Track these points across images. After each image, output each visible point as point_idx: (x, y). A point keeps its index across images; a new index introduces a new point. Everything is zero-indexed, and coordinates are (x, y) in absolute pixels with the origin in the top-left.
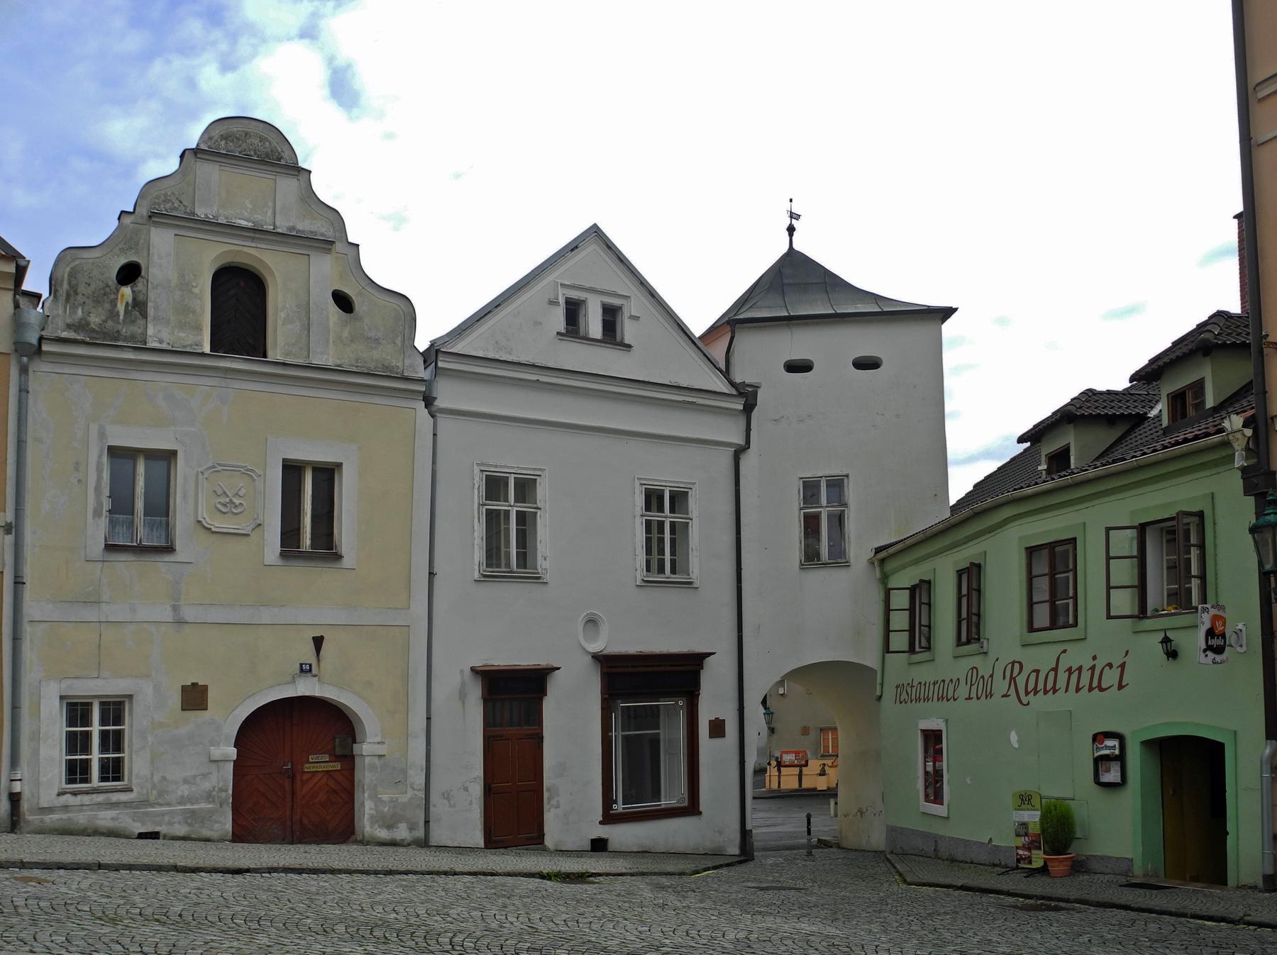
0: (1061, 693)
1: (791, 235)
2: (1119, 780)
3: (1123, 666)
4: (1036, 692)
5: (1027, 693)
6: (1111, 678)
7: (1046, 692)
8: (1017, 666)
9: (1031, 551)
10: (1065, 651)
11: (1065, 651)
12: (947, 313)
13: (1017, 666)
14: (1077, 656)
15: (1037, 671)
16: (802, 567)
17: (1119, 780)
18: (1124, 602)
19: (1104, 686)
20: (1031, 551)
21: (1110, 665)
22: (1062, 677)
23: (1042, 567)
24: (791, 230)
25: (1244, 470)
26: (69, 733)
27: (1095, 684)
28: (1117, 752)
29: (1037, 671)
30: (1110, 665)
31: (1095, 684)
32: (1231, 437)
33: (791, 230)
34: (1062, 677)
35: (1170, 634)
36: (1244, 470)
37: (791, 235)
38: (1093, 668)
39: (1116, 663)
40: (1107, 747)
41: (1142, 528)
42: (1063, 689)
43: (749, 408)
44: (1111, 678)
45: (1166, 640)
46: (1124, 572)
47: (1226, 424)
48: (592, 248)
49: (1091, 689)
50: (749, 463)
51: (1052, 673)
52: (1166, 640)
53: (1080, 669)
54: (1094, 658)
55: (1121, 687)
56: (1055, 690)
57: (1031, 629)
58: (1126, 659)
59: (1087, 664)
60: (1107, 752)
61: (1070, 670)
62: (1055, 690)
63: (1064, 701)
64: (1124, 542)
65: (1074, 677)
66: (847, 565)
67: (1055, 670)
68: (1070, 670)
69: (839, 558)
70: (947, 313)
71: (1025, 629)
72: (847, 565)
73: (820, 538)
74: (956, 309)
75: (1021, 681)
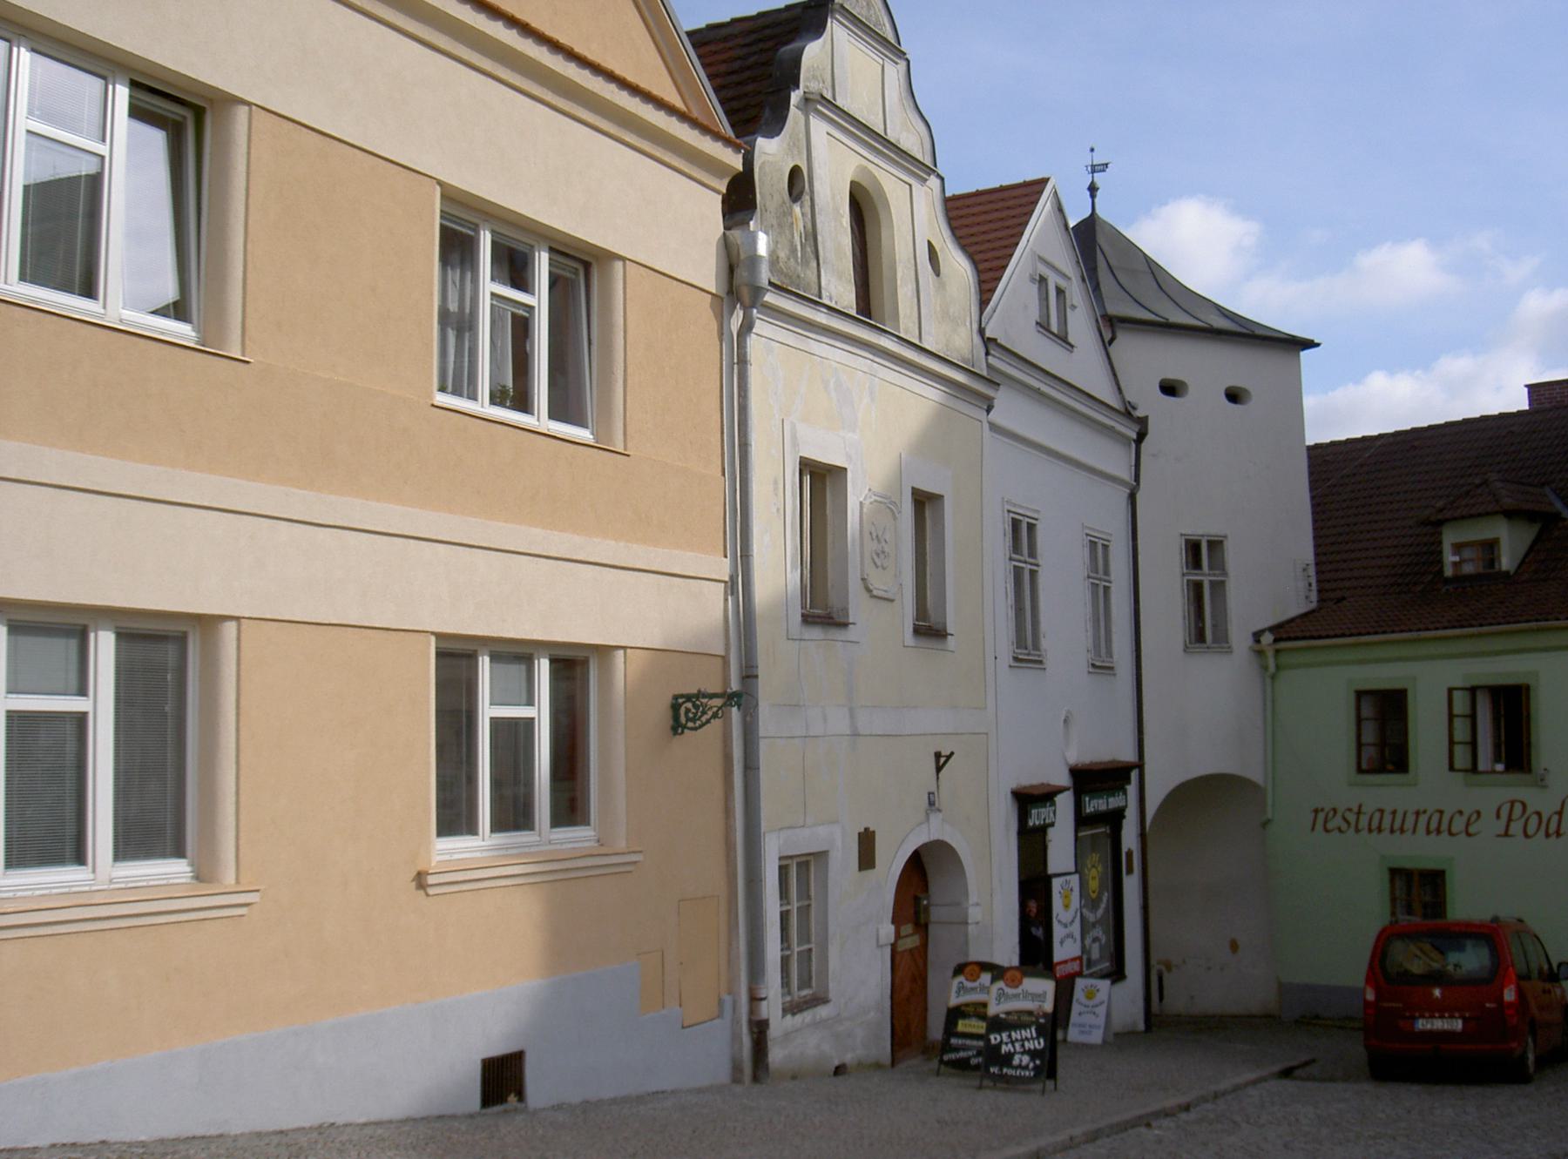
0: (1386, 833)
1: (1093, 196)
8: (1518, 808)
9: (1360, 694)
12: (1309, 344)
13: (1518, 808)
15: (1441, 812)
18: (1462, 757)
20: (1360, 694)
22: (1409, 824)
23: (1367, 711)
24: (1093, 189)
26: (12, 716)
29: (1441, 812)
33: (1093, 189)
34: (1409, 824)
37: (1093, 196)
41: (1473, 690)
43: (1141, 436)
46: (1462, 732)
48: (70, 729)
56: (1380, 830)
64: (1461, 704)
65: (1397, 825)
66: (1229, 651)
69: (1222, 638)
70: (1309, 344)
72: (1229, 651)
73: (1203, 623)
74: (1318, 345)
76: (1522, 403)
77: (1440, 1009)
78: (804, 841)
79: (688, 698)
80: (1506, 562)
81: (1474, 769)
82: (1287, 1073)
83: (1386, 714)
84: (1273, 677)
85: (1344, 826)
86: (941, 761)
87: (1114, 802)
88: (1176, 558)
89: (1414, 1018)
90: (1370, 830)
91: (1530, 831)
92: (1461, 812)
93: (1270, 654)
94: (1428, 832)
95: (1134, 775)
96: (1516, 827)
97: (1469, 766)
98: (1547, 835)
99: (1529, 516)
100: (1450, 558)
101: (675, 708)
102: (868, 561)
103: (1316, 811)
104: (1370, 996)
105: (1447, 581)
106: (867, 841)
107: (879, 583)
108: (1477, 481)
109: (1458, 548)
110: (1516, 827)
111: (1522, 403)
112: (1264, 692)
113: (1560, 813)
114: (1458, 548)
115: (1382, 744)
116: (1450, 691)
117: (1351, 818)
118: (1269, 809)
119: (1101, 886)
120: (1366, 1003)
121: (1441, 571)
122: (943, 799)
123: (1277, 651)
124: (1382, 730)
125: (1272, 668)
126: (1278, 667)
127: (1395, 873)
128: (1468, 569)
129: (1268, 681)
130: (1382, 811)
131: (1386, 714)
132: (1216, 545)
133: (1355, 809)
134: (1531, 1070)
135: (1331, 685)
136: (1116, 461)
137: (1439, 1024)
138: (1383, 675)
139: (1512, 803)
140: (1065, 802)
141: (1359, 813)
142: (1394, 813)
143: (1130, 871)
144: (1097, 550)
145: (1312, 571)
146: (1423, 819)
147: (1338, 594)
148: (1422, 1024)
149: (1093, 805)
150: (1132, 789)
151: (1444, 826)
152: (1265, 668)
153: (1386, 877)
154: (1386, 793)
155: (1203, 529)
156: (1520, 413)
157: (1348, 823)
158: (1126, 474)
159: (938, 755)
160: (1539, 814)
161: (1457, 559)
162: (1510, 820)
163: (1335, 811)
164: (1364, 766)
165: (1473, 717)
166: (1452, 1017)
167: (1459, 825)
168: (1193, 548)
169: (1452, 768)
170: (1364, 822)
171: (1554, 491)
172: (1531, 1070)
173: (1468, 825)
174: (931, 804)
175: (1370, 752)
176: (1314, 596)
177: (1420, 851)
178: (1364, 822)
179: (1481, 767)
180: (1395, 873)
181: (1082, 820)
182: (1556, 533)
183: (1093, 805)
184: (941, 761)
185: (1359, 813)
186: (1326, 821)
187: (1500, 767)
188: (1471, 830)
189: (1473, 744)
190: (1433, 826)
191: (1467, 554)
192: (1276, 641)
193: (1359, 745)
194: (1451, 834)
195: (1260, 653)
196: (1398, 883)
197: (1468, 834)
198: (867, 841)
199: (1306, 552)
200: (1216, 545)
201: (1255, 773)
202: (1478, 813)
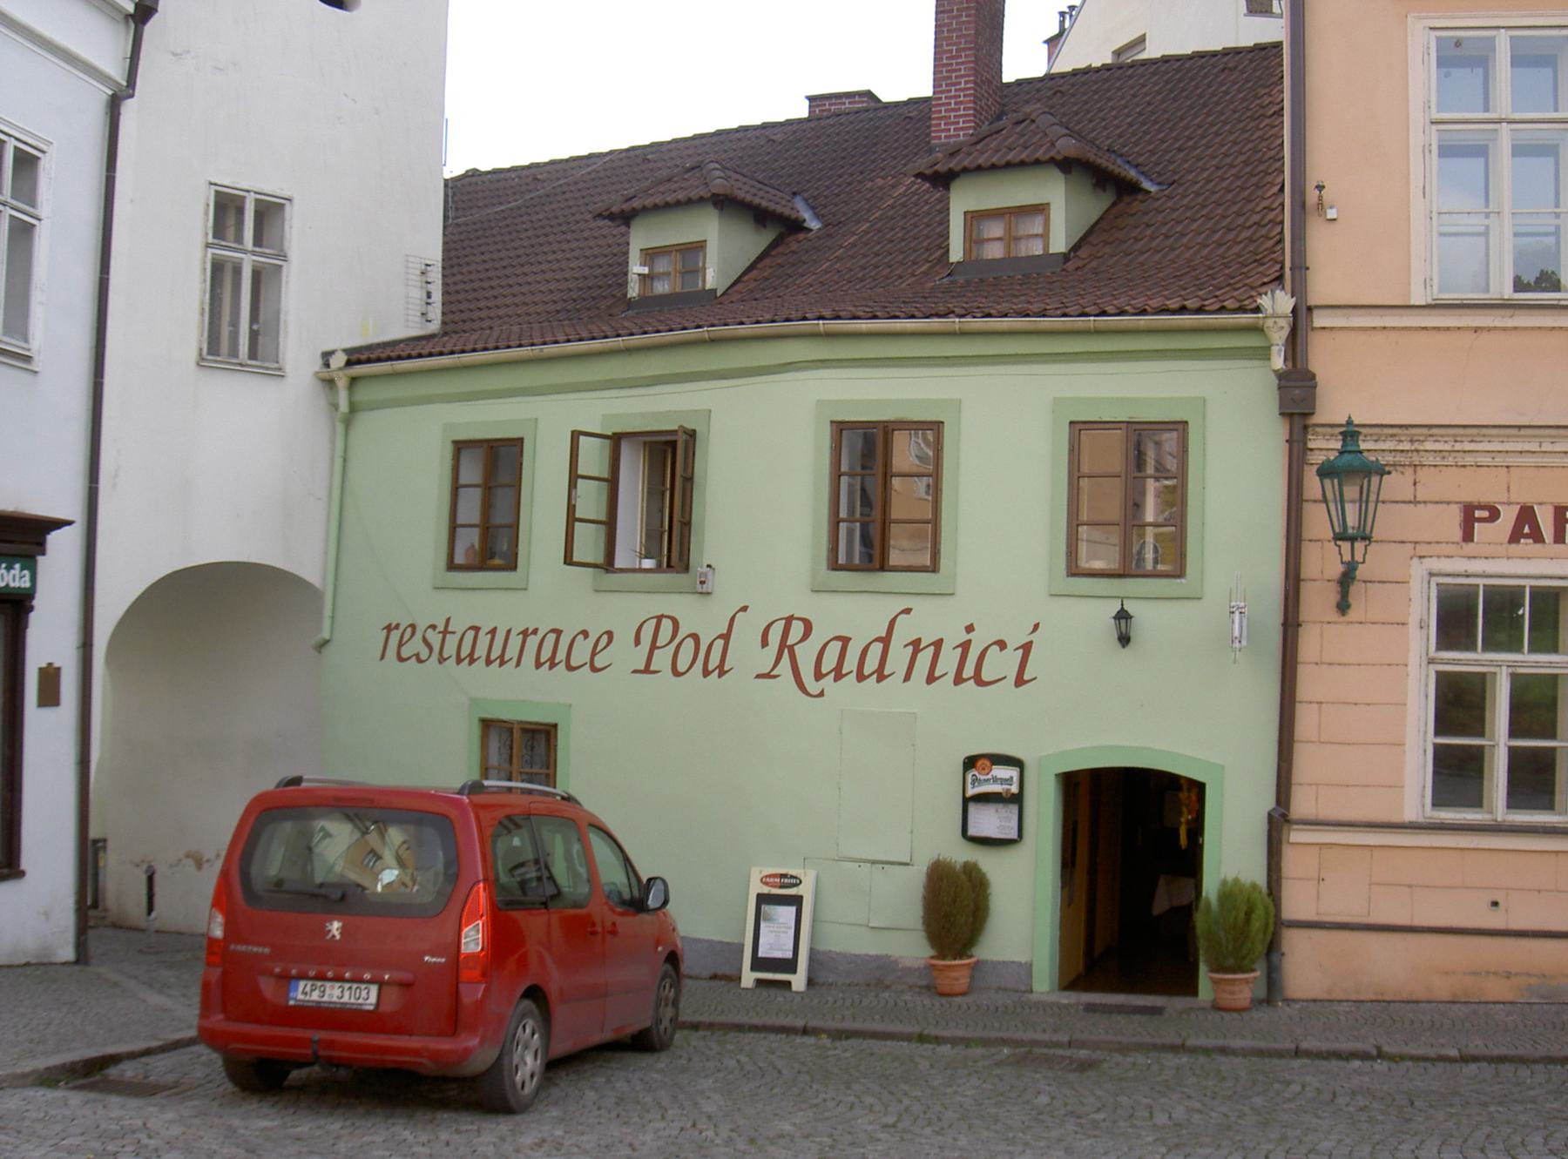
2: (1014, 835)
3: (1027, 648)
4: (838, 674)
5: (819, 676)
6: (1001, 665)
7: (861, 677)
8: (667, 625)
9: (460, 447)
10: (907, 611)
11: (907, 611)
13: (667, 625)
14: (931, 619)
15: (558, 632)
16: (201, 362)
17: (1014, 835)
18: (589, 543)
19: (985, 676)
20: (460, 447)
21: (585, 634)
22: (512, 652)
23: (472, 472)
25: (1281, 376)
26: (1437, 747)
27: (969, 671)
28: (1014, 789)
29: (558, 632)
30: (1002, 645)
31: (969, 671)
32: (1270, 322)
34: (512, 652)
35: (1130, 607)
36: (1281, 376)
38: (965, 646)
39: (1014, 641)
40: (995, 780)
41: (616, 440)
42: (514, 661)
44: (1001, 665)
45: (1123, 616)
46: (591, 500)
47: (1264, 301)
49: (959, 680)
50: (129, 109)
51: (720, 642)
52: (1123, 616)
53: (938, 644)
54: (970, 629)
55: (1020, 681)
57: (452, 566)
58: (1034, 637)
59: (956, 636)
60: (997, 788)
61: (916, 645)
62: (881, 676)
63: (898, 696)
64: (593, 458)
67: (886, 641)
68: (916, 645)
71: (824, 564)
73: (238, 324)
75: (806, 655)
76: (802, 111)
77: (333, 963)
78: (49, 713)
80: (712, 278)
82: (90, 1073)
84: (348, 422)
85: (424, 653)
89: (287, 979)
90: (459, 661)
91: (681, 667)
92: (585, 634)
93: (342, 383)
94: (538, 665)
96: (662, 659)
97: (600, 560)
98: (706, 673)
99: (761, 217)
100: (637, 268)
103: (389, 628)
104: (218, 932)
105: (630, 304)
109: (650, 255)
110: (662, 659)
111: (802, 111)
112: (333, 442)
113: (726, 637)
114: (650, 255)
115: (487, 529)
116: (576, 436)
117: (435, 639)
118: (327, 623)
120: (212, 942)
121: (624, 285)
123: (354, 380)
124: (487, 506)
125: (344, 406)
127: (487, 724)
128: (662, 288)
129: (340, 428)
130: (477, 629)
131: (494, 465)
132: (270, 212)
133: (441, 628)
134: (1487, 817)
135: (416, 439)
136: (103, 46)
137: (334, 994)
138: (489, 417)
139: (659, 618)
141: (445, 632)
142: (493, 632)
145: (436, 275)
146: (532, 642)
148: (305, 993)
151: (561, 655)
152: (336, 407)
153: (476, 730)
154: (485, 604)
155: (254, 178)
156: (800, 121)
157: (431, 649)
158: (118, 73)
160: (695, 637)
161: (646, 270)
162: (653, 647)
163: (413, 626)
164: (459, 559)
165: (613, 482)
166: (357, 980)
167: (581, 654)
168: (226, 207)
169: (568, 560)
170: (450, 649)
171: (806, 200)
172: (1487, 817)
173: (594, 654)
175: (470, 539)
176: (436, 312)
177: (523, 693)
178: (450, 649)
179: (619, 563)
180: (487, 724)
182: (794, 246)
185: (445, 632)
186: (400, 645)
187: (648, 563)
188: (598, 663)
189: (610, 524)
190: (546, 654)
191: (662, 265)
192: (349, 363)
193: (454, 527)
194: (570, 668)
195: (330, 383)
196: (494, 745)
197: (594, 669)
199: (432, 247)
200: (270, 212)
201: (308, 564)
202: (610, 634)
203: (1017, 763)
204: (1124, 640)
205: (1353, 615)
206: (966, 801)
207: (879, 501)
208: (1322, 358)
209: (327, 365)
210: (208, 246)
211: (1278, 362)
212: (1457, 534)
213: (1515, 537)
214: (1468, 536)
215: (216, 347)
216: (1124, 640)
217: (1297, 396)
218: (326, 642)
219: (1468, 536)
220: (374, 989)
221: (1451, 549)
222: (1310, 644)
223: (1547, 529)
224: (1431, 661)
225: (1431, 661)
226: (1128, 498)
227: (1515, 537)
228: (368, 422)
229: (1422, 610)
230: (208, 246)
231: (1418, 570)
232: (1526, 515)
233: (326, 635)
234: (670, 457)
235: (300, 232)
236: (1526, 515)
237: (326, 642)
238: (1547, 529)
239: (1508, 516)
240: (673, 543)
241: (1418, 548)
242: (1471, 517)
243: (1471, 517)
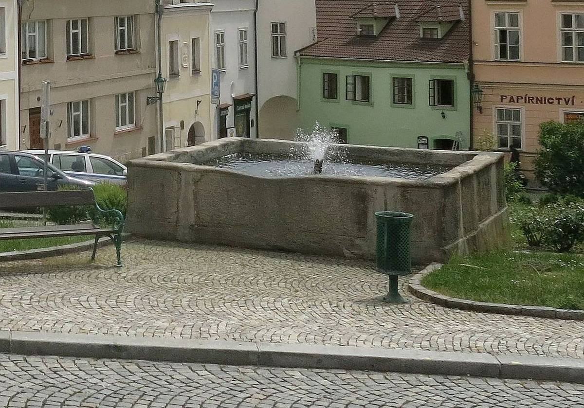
35: (444, 111)
41: (355, 77)
45: (443, 113)
52: (443, 113)
64: (350, 81)
69: (283, 54)
73: (278, 50)
79: (150, 98)
81: (354, 99)
83: (331, 81)
86: (198, 103)
87: (247, 107)
88: (270, 29)
95: (254, 99)
101: (148, 100)
102: (182, 59)
106: (182, 124)
107: (185, 65)
108: (369, 4)
114: (361, 26)
119: (243, 129)
122: (199, 112)
126: (301, 63)
131: (331, 81)
132: (282, 25)
135: (315, 74)
140: (231, 110)
143: (252, 126)
144: (242, 34)
147: (325, 36)
149: (239, 108)
150: (253, 102)
152: (298, 63)
155: (278, 20)
159: (198, 101)
161: (361, 30)
165: (354, 84)
168: (275, 26)
169: (347, 99)
174: (196, 113)
181: (236, 112)
183: (239, 108)
184: (198, 103)
189: (354, 92)
197: (364, 343)
198: (182, 124)
200: (282, 25)
201: (294, 95)
203: (427, 138)
204: (444, 117)
205: (483, 114)
206: (419, 144)
207: (403, 91)
208: (477, 70)
209: (296, 55)
210: (272, 35)
211: (466, 71)
212: (500, 100)
213: (510, 101)
214: (502, 101)
215: (275, 54)
216: (444, 117)
217: (471, 77)
218: (298, 110)
219: (502, 101)
220: (430, 35)
221: (499, 103)
222: (475, 119)
223: (516, 101)
224: (497, 122)
225: (497, 122)
226: (444, 93)
227: (510, 101)
228: (304, 66)
229: (495, 113)
230: (272, 35)
231: (493, 107)
232: (512, 98)
233: (298, 109)
234: (366, 81)
235: (288, 28)
236: (512, 98)
237: (298, 110)
238: (516, 101)
239: (509, 98)
240: (366, 96)
241: (494, 103)
242: (502, 98)
243: (502, 98)
